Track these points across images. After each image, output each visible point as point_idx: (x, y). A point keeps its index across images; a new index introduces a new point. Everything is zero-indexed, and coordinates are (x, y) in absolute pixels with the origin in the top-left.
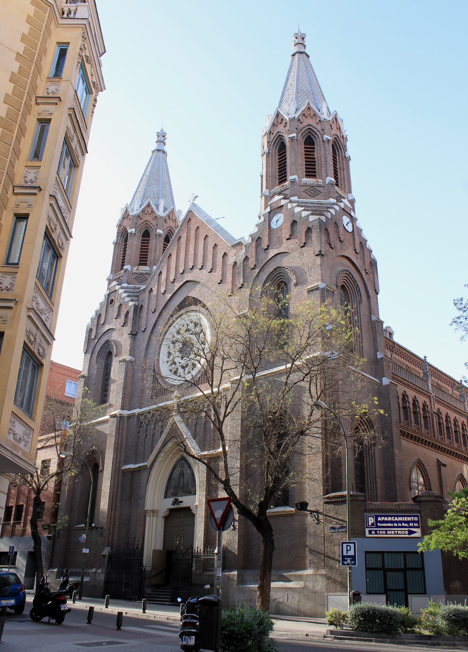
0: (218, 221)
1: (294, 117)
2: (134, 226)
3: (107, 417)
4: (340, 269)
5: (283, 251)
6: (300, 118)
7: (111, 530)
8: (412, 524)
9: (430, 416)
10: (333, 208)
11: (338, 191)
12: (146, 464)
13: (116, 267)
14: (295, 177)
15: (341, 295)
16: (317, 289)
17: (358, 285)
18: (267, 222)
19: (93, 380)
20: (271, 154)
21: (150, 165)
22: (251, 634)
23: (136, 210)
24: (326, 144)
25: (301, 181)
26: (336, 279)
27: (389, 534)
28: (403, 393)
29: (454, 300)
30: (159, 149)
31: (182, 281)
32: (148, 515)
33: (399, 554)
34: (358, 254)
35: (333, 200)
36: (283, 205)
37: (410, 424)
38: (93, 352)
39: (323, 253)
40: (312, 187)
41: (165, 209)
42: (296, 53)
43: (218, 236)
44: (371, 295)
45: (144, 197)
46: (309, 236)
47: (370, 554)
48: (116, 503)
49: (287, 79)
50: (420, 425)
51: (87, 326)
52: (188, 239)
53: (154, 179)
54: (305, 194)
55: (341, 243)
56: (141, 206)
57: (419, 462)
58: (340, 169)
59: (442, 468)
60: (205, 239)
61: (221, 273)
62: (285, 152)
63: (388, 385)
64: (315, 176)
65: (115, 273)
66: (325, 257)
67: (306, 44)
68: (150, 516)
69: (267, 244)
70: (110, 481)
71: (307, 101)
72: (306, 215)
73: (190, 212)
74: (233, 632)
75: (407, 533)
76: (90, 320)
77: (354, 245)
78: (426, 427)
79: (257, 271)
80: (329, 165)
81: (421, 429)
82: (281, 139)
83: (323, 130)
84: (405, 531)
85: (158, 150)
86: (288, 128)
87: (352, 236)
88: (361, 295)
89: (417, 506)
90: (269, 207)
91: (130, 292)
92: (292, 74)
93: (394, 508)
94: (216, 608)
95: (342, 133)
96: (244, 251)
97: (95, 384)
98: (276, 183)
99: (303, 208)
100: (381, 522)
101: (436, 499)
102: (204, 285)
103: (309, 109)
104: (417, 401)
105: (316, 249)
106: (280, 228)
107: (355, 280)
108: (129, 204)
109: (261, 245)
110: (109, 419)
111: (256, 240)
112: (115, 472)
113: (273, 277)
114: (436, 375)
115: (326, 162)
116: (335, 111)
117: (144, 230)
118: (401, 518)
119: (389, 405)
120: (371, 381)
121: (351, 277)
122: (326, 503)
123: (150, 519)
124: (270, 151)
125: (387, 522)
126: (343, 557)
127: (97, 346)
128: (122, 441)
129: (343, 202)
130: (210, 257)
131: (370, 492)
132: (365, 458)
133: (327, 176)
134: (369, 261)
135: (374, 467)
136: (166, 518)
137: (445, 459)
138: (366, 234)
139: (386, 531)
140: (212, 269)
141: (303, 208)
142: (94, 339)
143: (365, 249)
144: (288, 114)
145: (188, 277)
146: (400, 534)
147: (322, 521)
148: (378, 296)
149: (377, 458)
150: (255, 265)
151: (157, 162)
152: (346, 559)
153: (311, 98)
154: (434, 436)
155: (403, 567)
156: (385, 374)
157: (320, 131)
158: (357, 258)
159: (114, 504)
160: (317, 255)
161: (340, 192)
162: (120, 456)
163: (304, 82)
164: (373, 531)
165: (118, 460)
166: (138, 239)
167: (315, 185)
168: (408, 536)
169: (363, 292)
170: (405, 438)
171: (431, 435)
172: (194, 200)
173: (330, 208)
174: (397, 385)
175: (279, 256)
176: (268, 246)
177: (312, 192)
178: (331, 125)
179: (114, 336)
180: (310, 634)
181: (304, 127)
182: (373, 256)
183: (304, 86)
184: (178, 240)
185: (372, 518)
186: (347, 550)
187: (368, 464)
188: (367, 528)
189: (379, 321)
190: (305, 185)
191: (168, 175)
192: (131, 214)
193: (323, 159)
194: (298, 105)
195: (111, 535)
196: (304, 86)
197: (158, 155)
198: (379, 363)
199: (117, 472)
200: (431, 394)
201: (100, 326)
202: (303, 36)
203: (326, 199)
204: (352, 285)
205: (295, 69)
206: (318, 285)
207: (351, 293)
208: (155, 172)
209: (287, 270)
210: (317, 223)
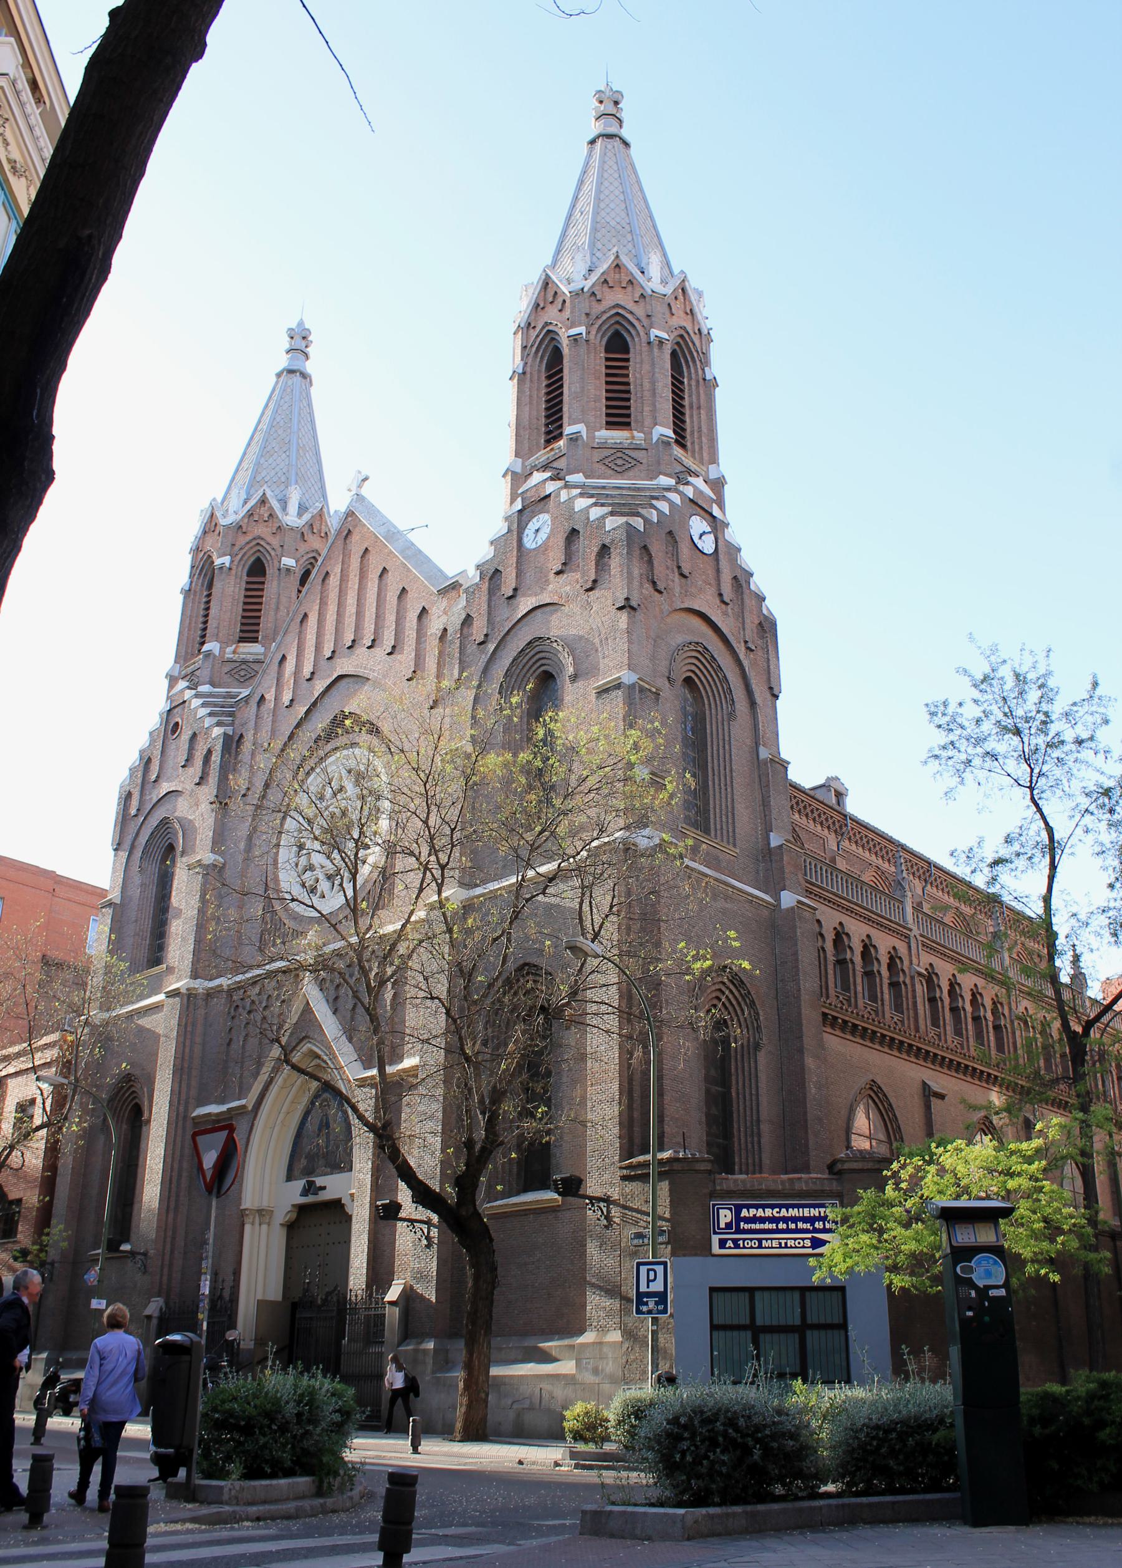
0: (412, 537)
2: (228, 549)
3: (161, 997)
4: (680, 639)
5: (548, 601)
6: (596, 290)
7: (167, 1257)
9: (908, 981)
10: (665, 498)
12: (243, 1102)
13: (187, 647)
14: (580, 427)
15: (686, 700)
16: (618, 686)
17: (725, 676)
18: (515, 533)
19: (132, 914)
20: (528, 376)
21: (271, 406)
22: (272, 1420)
24: (656, 350)
25: (594, 438)
26: (668, 663)
28: (835, 929)
29: (927, 705)
30: (291, 368)
31: (330, 676)
33: (788, 1294)
34: (727, 604)
35: (665, 481)
36: (549, 495)
37: (853, 1000)
38: (133, 847)
39: (634, 603)
40: (620, 450)
41: (302, 509)
42: (598, 137)
43: (409, 570)
44: (759, 700)
45: (253, 483)
46: (605, 565)
47: (721, 1294)
48: (178, 1196)
49: (576, 199)
51: (121, 787)
52: (344, 578)
54: (604, 467)
55: (683, 580)
56: (245, 503)
58: (691, 407)
59: (934, 1101)
60: (381, 576)
61: (413, 654)
62: (561, 371)
63: (792, 908)
64: (628, 424)
65: (186, 661)
67: (624, 115)
68: (253, 1224)
69: (513, 586)
70: (163, 1145)
71: (615, 250)
73: (350, 514)
74: (231, 1413)
76: (127, 773)
77: (719, 585)
78: (898, 1007)
79: (491, 647)
82: (552, 339)
84: (803, 1239)
85: (291, 372)
86: (567, 313)
87: (712, 563)
89: (835, 1183)
91: (216, 706)
92: (586, 187)
93: (780, 1187)
94: (186, 1358)
95: (699, 323)
96: (463, 602)
97: (136, 921)
98: (538, 444)
99: (592, 500)
100: (748, 1220)
102: (377, 684)
104: (874, 947)
105: (618, 594)
106: (544, 548)
108: (219, 500)
109: (499, 589)
110: (163, 1001)
112: (177, 1123)
113: (525, 661)
116: (682, 272)
117: (253, 559)
119: (796, 954)
120: (752, 900)
122: (624, 1178)
124: (528, 369)
125: (762, 1220)
126: (640, 1295)
127: (142, 832)
128: (191, 1050)
130: (390, 618)
131: (743, 1156)
132: (734, 1078)
133: (656, 424)
134: (757, 622)
135: (754, 1098)
136: (291, 1227)
137: (939, 1081)
138: (749, 558)
139: (760, 1241)
140: (394, 647)
141: (592, 500)
142: (135, 816)
143: (746, 591)
144: (569, 281)
145: (344, 666)
147: (617, 1220)
148: (779, 703)
149: (762, 1077)
150: (486, 635)
151: (287, 398)
154: (917, 1030)
155: (798, 1322)
156: (787, 883)
157: (643, 319)
158: (725, 614)
159: (173, 1199)
160: (620, 608)
161: (689, 462)
162: (189, 1086)
163: (612, 206)
165: (183, 1096)
167: (626, 446)
168: (810, 1251)
169: (739, 693)
170: (838, 1032)
171: (909, 1027)
172: (360, 486)
173: (656, 498)
174: (815, 909)
175: (539, 612)
176: (515, 590)
177: (620, 462)
179: (182, 808)
180: (525, 1461)
181: (604, 312)
182: (768, 609)
183: (613, 214)
184: (324, 580)
185: (728, 1212)
186: (649, 1281)
188: (715, 1233)
190: (602, 447)
191: (314, 429)
192: (223, 522)
194: (595, 259)
195: (166, 1271)
196: (613, 214)
198: (773, 858)
199: (180, 1123)
200: (911, 930)
201: (148, 787)
202: (616, 97)
203: (651, 479)
205: (594, 173)
206: (619, 678)
207: (708, 697)
209: (555, 645)
210: (621, 535)
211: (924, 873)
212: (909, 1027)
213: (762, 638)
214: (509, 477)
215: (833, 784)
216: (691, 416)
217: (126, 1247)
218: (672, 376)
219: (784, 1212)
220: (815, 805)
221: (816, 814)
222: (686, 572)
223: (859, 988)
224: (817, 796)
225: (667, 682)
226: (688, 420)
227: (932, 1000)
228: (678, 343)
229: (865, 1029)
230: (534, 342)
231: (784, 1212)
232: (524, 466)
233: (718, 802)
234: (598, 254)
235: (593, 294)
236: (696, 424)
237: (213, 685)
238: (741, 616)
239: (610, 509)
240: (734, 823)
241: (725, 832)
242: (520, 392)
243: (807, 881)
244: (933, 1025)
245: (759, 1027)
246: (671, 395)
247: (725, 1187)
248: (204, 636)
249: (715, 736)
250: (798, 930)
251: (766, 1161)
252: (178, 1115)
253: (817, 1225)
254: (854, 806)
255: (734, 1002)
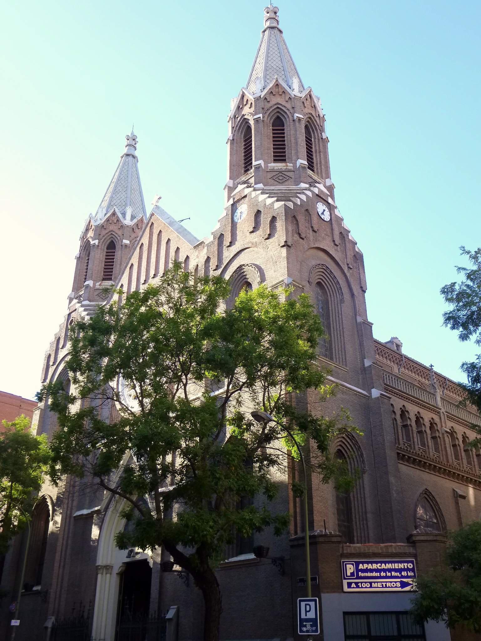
1: (260, 96)
2: (97, 237)
4: (314, 263)
7: (58, 593)
8: (405, 572)
10: (304, 193)
11: (313, 176)
14: (261, 162)
15: (318, 294)
18: (230, 215)
20: (235, 141)
21: (118, 171)
23: (101, 219)
24: (297, 124)
25: (268, 167)
27: (374, 587)
30: (128, 153)
32: (100, 572)
34: (337, 246)
37: (412, 446)
39: (289, 244)
41: (133, 217)
44: (356, 293)
45: (110, 205)
50: (427, 447)
53: (122, 186)
54: (273, 181)
55: (314, 233)
56: (105, 215)
57: (428, 494)
58: (316, 152)
63: (378, 398)
66: (292, 248)
67: (279, 19)
72: (278, 206)
75: (400, 585)
77: (333, 236)
78: (437, 449)
80: (300, 147)
81: (429, 452)
83: (293, 108)
84: (396, 582)
88: (342, 293)
90: (232, 199)
91: (91, 310)
93: (380, 551)
95: (319, 112)
96: (205, 250)
100: (363, 571)
101: (435, 539)
103: (277, 87)
104: (422, 418)
107: (335, 276)
111: (218, 237)
114: (458, 392)
115: (296, 143)
116: (309, 87)
118: (390, 564)
119: (381, 421)
121: (329, 272)
123: (102, 577)
124: (235, 138)
125: (371, 571)
129: (317, 187)
131: (359, 532)
134: (353, 255)
135: (363, 499)
138: (347, 224)
139: (371, 583)
143: (347, 240)
146: (389, 587)
151: (126, 167)
152: (305, 623)
153: (281, 75)
154: (448, 461)
156: (375, 385)
158: (336, 250)
160: (283, 246)
161: (315, 177)
164: (353, 584)
166: (102, 251)
167: (284, 170)
168: (400, 589)
169: (345, 290)
171: (443, 460)
173: (300, 193)
174: (390, 398)
177: (281, 178)
178: (303, 102)
181: (271, 107)
182: (358, 248)
183: (275, 63)
186: (306, 612)
187: (355, 496)
188: (345, 579)
189: (366, 322)
190: (272, 171)
193: (293, 141)
194: (266, 83)
196: (275, 63)
197: (127, 160)
200: (440, 409)
202: (276, 10)
203: (297, 185)
204: (331, 281)
205: (264, 46)
208: (123, 179)
211: (443, 384)
212: (443, 460)
213: (356, 262)
214: (227, 190)
215: (394, 341)
216: (316, 156)
217: (37, 588)
218: (306, 137)
219: (383, 566)
220: (386, 350)
221: (387, 355)
222: (316, 229)
223: (416, 440)
224: (387, 346)
225: (308, 284)
226: (314, 157)
227: (454, 446)
228: (308, 121)
229: (420, 461)
230: (238, 124)
231: (383, 566)
232: (234, 184)
233: (336, 344)
234: (268, 81)
235: (266, 99)
236: (318, 160)
237: (90, 301)
238: (345, 251)
239: (276, 198)
240: (345, 355)
241: (341, 360)
242: (231, 149)
243: (385, 384)
244: (455, 459)
245: (363, 460)
246: (305, 146)
247: (349, 551)
248: (86, 279)
249: (334, 311)
250: (382, 409)
251: (371, 534)
252: (66, 515)
253: (403, 573)
254: (405, 351)
255: (350, 448)
